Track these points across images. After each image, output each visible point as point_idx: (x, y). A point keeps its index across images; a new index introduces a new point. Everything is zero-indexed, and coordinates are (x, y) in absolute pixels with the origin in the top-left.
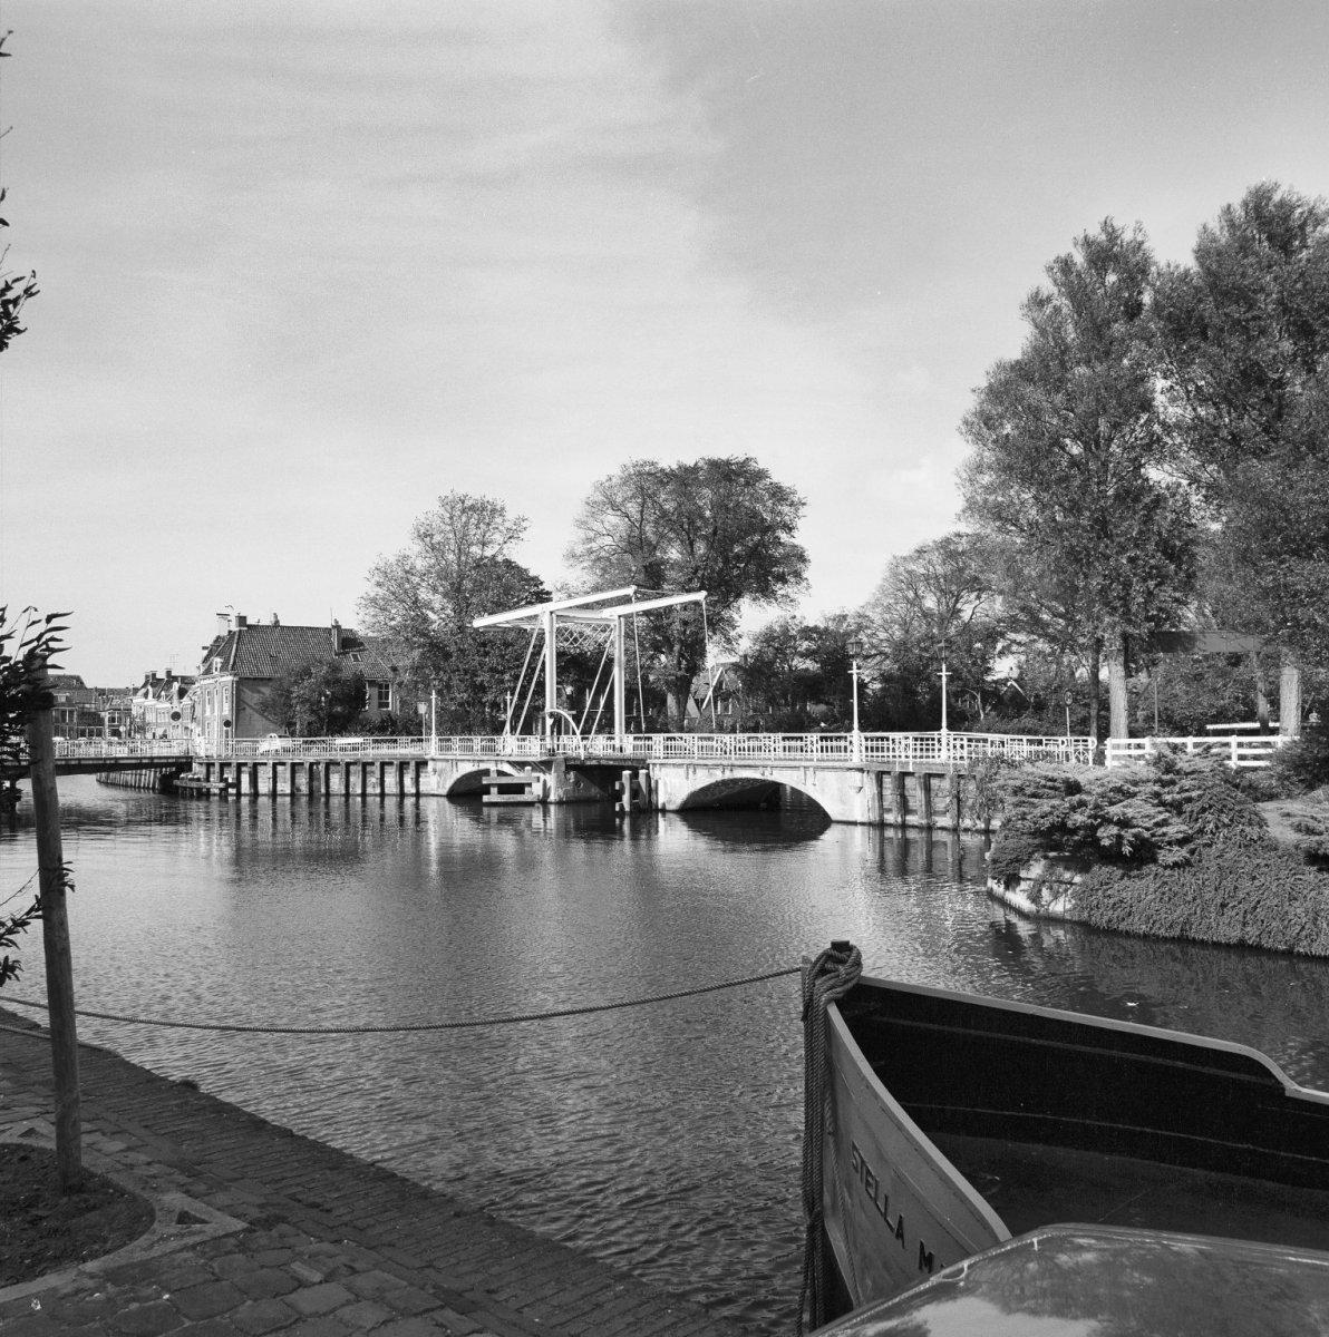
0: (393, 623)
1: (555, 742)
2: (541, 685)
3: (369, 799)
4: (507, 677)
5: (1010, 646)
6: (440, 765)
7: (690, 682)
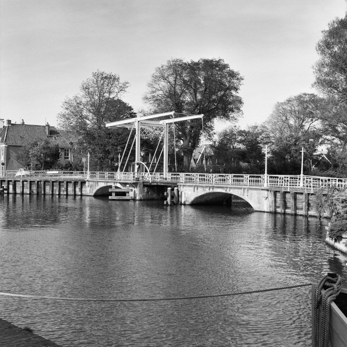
0: (72, 124)
1: (139, 175)
2: (134, 151)
3: (62, 197)
4: (119, 148)
5: (324, 141)
6: (91, 183)
7: (192, 152)
